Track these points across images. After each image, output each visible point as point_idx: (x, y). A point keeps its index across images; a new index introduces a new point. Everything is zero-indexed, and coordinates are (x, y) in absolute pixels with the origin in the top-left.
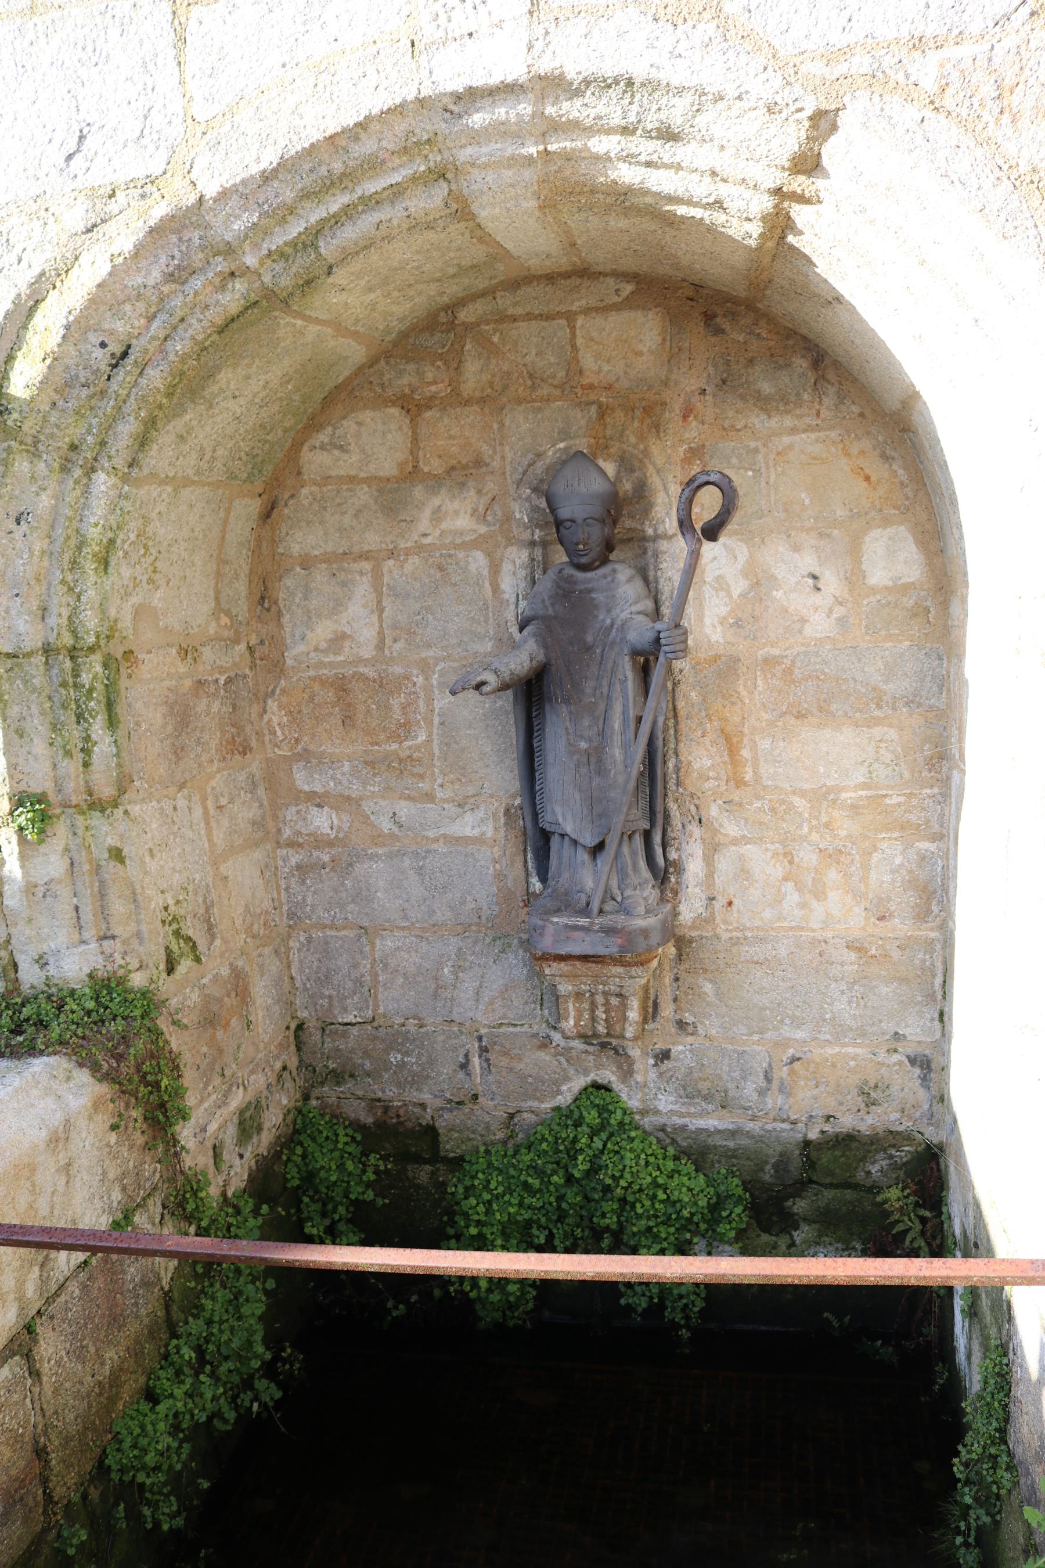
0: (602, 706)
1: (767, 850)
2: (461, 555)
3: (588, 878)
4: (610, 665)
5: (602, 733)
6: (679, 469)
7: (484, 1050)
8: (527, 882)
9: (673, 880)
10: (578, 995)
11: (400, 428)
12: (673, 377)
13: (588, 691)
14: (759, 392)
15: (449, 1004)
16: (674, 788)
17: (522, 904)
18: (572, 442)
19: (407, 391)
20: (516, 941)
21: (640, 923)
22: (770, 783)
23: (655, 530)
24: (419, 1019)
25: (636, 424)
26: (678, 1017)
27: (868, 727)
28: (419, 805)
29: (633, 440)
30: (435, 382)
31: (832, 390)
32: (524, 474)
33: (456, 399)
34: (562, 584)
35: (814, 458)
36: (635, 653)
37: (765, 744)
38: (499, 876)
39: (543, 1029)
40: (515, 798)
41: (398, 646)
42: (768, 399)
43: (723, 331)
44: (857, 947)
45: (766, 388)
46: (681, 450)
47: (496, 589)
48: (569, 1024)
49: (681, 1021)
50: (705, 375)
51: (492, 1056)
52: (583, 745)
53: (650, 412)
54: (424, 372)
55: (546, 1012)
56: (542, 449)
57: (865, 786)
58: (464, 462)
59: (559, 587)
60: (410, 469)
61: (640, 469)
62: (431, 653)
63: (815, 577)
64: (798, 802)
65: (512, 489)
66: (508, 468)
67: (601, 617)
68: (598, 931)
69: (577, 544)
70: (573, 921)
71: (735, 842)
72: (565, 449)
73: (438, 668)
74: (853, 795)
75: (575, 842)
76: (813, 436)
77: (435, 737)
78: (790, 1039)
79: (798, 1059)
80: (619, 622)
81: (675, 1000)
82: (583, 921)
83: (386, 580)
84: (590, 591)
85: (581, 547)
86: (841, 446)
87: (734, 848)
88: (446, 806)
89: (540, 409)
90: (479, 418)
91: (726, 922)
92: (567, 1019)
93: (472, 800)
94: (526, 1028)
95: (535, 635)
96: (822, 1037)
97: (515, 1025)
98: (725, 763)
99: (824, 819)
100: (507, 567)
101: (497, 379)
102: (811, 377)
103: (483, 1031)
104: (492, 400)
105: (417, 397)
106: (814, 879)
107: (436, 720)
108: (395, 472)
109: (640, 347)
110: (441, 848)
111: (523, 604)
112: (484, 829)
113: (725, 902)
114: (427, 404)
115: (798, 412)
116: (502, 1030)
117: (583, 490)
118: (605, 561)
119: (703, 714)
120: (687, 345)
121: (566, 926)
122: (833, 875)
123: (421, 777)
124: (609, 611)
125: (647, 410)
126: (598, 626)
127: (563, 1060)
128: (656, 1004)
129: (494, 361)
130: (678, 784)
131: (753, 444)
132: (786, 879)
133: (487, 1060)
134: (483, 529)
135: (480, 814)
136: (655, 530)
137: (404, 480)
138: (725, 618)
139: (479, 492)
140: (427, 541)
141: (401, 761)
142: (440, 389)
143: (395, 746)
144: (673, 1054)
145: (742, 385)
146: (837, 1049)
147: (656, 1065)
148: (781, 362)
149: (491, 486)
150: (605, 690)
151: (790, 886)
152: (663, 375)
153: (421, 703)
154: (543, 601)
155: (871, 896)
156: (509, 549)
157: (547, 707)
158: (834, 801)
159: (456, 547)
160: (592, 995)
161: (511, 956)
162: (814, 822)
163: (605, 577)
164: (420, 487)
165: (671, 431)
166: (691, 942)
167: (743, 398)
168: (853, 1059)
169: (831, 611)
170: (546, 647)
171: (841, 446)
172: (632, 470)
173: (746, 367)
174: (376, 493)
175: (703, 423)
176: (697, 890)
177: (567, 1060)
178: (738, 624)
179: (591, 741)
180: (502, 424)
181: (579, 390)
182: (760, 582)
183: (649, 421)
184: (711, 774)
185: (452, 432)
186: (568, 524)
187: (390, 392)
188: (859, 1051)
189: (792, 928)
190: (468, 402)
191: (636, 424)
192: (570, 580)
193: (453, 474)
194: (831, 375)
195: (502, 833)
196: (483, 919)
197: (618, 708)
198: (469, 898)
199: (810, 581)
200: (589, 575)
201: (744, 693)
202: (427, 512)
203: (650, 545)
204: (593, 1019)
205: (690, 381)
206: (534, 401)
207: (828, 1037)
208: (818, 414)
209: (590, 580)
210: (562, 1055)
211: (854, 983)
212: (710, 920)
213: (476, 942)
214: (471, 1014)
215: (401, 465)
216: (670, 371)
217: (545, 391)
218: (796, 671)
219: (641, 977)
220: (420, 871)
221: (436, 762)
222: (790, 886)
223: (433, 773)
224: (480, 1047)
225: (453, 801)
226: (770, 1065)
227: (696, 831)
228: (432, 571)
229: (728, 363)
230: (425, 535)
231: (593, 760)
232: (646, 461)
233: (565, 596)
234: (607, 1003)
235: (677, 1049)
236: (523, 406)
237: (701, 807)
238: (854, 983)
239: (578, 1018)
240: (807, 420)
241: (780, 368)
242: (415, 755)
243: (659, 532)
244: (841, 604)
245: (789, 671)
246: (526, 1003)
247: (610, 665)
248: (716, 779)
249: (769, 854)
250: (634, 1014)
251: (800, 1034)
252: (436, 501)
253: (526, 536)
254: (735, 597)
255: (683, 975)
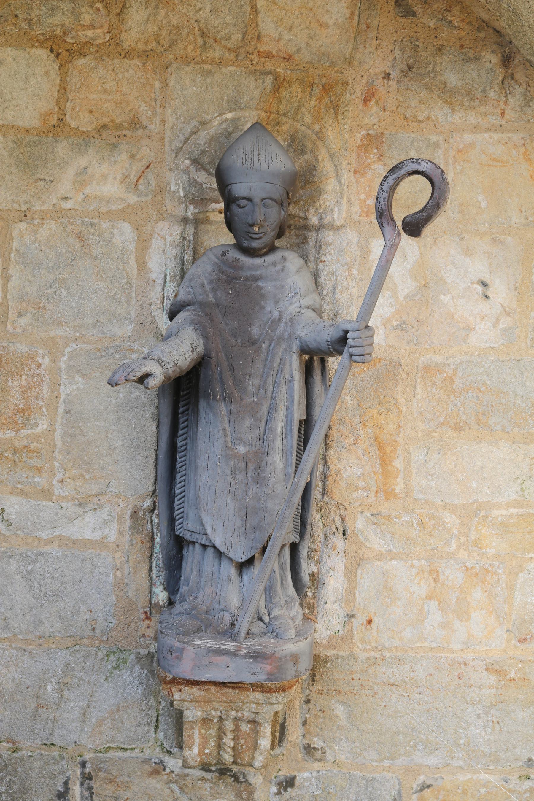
0: (265, 408)
1: (412, 566)
2: (105, 225)
3: (232, 594)
4: (277, 362)
5: (263, 437)
6: (354, 155)
7: (87, 777)
8: (150, 591)
9: (310, 594)
10: (206, 721)
11: (47, 73)
12: (358, 56)
13: (251, 389)
14: (445, 84)
15: (50, 725)
16: (319, 496)
17: (143, 616)
18: (240, 113)
19: (58, 32)
20: (132, 657)
21: (291, 648)
22: (421, 496)
23: (321, 219)
24: (14, 743)
25: (313, 102)
26: (306, 742)
27: (525, 443)
28: (33, 502)
29: (308, 119)
30: (92, 27)
31: (519, 91)
32: (185, 142)
33: (114, 48)
34: (225, 269)
35: (494, 160)
36: (303, 351)
37: (419, 456)
38: (120, 585)
39: (157, 754)
40: (144, 499)
41: (23, 321)
42: (453, 92)
43: (414, 14)
44: (496, 670)
45: (453, 80)
46: (359, 136)
47: (142, 266)
48: (193, 753)
49: (309, 746)
50: (391, 58)
51: (96, 784)
52: (242, 449)
53: (330, 92)
54: (80, 14)
55: (161, 735)
56: (207, 117)
57: (516, 504)
58: (118, 121)
59: (221, 271)
60: (55, 122)
61: (312, 151)
62: (60, 332)
63: (485, 285)
64: (448, 517)
65: (169, 158)
66: (168, 133)
67: (268, 309)
68: (245, 657)
69: (252, 225)
70: (216, 644)
71: (380, 557)
72: (233, 120)
73: (68, 349)
74: (504, 512)
75: (219, 554)
76: (496, 136)
77: (58, 426)
78: (421, 765)
79: (429, 786)
80: (287, 316)
81: (305, 723)
82: (229, 645)
83: (15, 244)
84: (257, 279)
85: (256, 229)
86: (522, 150)
87: (378, 563)
88: (64, 504)
89: (209, 72)
90: (139, 74)
91: (364, 641)
92: (190, 747)
93: (95, 500)
94: (136, 753)
95: (193, 323)
96: (455, 763)
97: (125, 750)
98: (375, 473)
99: (473, 536)
100: (156, 244)
101: (164, 33)
102: (500, 73)
103: (88, 756)
104: (155, 56)
105: (69, 40)
106: (458, 599)
107: (61, 408)
108: (36, 123)
109: (326, 18)
110: (55, 550)
111: (171, 287)
112: (107, 531)
113: (365, 620)
114: (81, 50)
115: (483, 109)
116: (110, 755)
117: (264, 167)
118: (272, 249)
119: (357, 420)
120: (376, 23)
121: (210, 650)
122: (478, 594)
123: (39, 470)
124: (276, 303)
125: (327, 89)
126: (264, 318)
127: (175, 788)
128: (283, 728)
129: (163, 12)
130: (324, 493)
131: (434, 138)
132: (429, 597)
133: (90, 789)
134: (133, 199)
135: (103, 515)
136: (321, 219)
137: (46, 133)
138: (389, 320)
139: (132, 156)
140: (68, 205)
141: (15, 451)
142: (98, 34)
143: (10, 434)
144: (297, 782)
145: (428, 74)
146: (469, 776)
147: (279, 793)
148: (471, 54)
149: (147, 152)
150: (269, 390)
151: (433, 603)
152: (347, 52)
153: (45, 387)
154: (203, 285)
155: (514, 617)
156: (161, 224)
157: (202, 404)
158: (485, 518)
159: (100, 215)
160: (221, 719)
161: (126, 674)
162: (463, 539)
163: (274, 264)
164: (65, 143)
165: (349, 115)
166: (325, 662)
167: (427, 87)
168: (484, 786)
169: (497, 320)
170: (206, 337)
171: (522, 150)
172: (303, 152)
173: (434, 55)
174: (12, 145)
175: (384, 109)
176: (336, 607)
177: (181, 788)
178: (402, 327)
179: (250, 445)
180: (165, 84)
181: (255, 57)
182: (428, 285)
183: (327, 100)
184: (360, 484)
185: (107, 86)
186: (243, 202)
187: (38, 30)
188: (489, 777)
189: (431, 649)
190: (127, 55)
191: (313, 102)
192: (235, 266)
193: (105, 133)
194: (520, 75)
195: (127, 538)
196: (98, 631)
197: (282, 410)
198: (83, 608)
199: (480, 288)
200: (257, 261)
201: (402, 400)
202: (71, 172)
203: (312, 236)
204: (220, 747)
205: (376, 61)
206: (203, 62)
207: (461, 763)
208: (503, 114)
209: (259, 267)
210: (176, 782)
211: (492, 706)
212: (348, 639)
213: (87, 657)
214: (74, 737)
215: (45, 116)
216: (355, 49)
217: (217, 53)
218: (458, 381)
219: (278, 703)
220: (28, 576)
221: (57, 454)
222: (433, 603)
223: (53, 467)
224: (83, 774)
225: (74, 499)
226: (399, 793)
227: (337, 541)
228: (71, 240)
229: (416, 48)
230: (66, 199)
231: (251, 467)
232: (320, 144)
233: (228, 282)
234: (237, 729)
235: (302, 776)
236: (192, 65)
237: (347, 518)
238: (492, 706)
239: (203, 746)
240: (492, 119)
241: (468, 60)
242: (32, 446)
243: (326, 222)
244: (508, 314)
245: (450, 380)
246: (139, 725)
247: (277, 362)
248: (365, 489)
249: (414, 571)
250: (265, 743)
251: (432, 761)
252: (82, 162)
253: (179, 211)
254: (401, 298)
255: (314, 697)
